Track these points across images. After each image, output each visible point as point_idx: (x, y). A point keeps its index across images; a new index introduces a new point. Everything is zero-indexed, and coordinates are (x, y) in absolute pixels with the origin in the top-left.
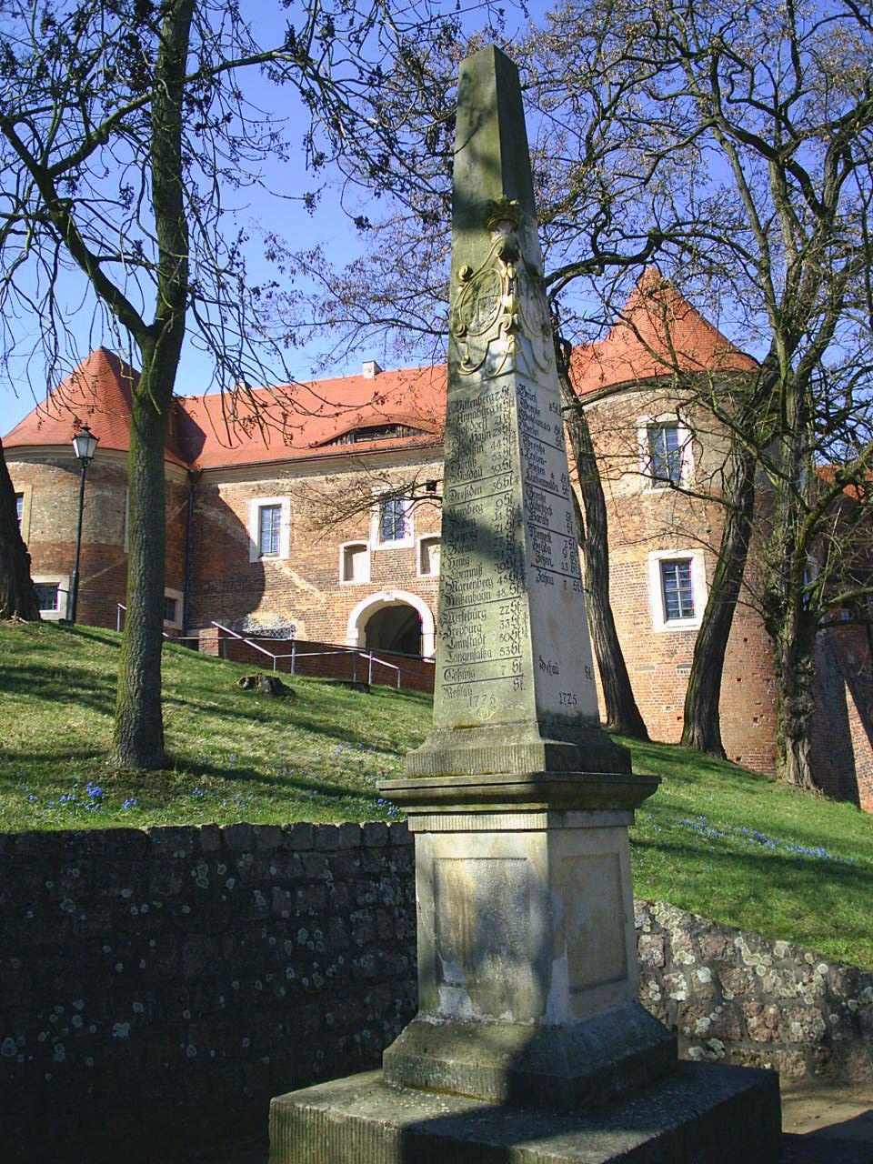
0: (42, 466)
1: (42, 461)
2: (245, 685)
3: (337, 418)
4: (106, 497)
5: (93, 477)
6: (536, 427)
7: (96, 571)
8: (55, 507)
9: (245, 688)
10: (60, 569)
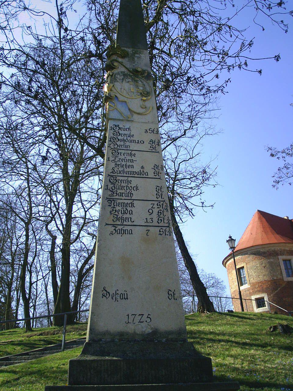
0: (247, 255)
1: (247, 254)
2: (271, 330)
3: (201, 195)
4: (272, 262)
5: (265, 255)
6: (128, 144)
7: (276, 290)
8: (255, 269)
9: (272, 331)
10: (263, 291)
